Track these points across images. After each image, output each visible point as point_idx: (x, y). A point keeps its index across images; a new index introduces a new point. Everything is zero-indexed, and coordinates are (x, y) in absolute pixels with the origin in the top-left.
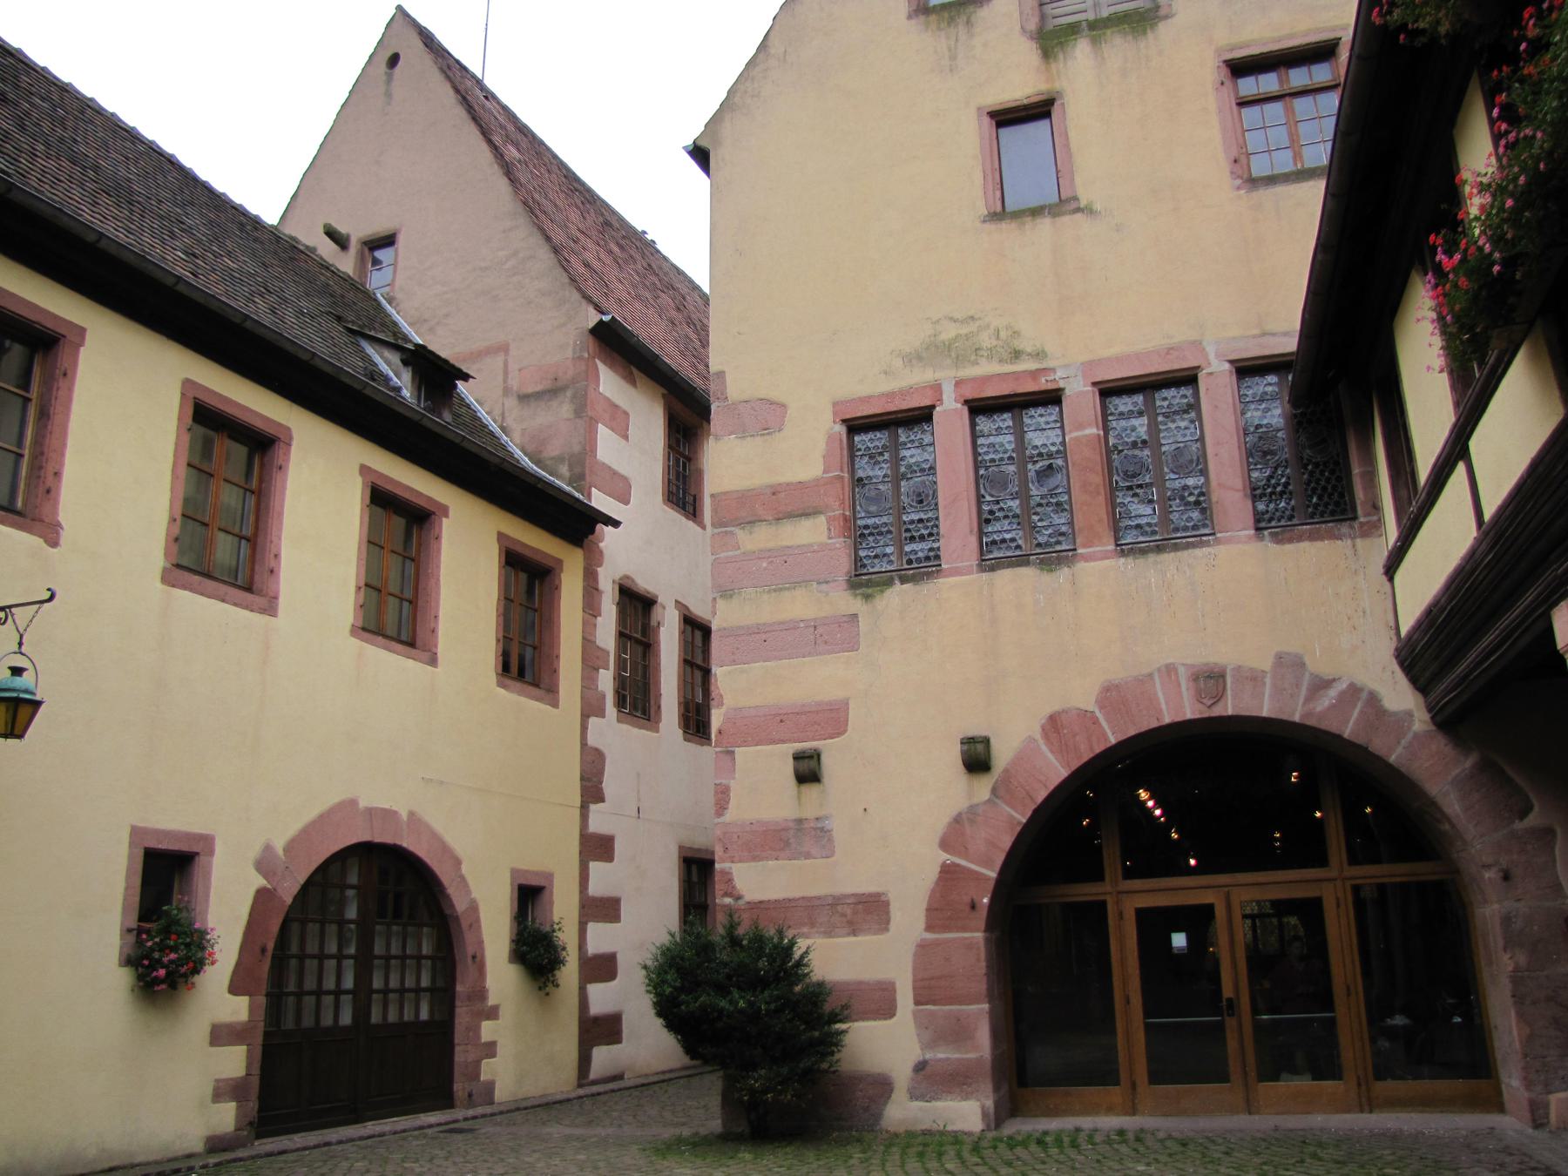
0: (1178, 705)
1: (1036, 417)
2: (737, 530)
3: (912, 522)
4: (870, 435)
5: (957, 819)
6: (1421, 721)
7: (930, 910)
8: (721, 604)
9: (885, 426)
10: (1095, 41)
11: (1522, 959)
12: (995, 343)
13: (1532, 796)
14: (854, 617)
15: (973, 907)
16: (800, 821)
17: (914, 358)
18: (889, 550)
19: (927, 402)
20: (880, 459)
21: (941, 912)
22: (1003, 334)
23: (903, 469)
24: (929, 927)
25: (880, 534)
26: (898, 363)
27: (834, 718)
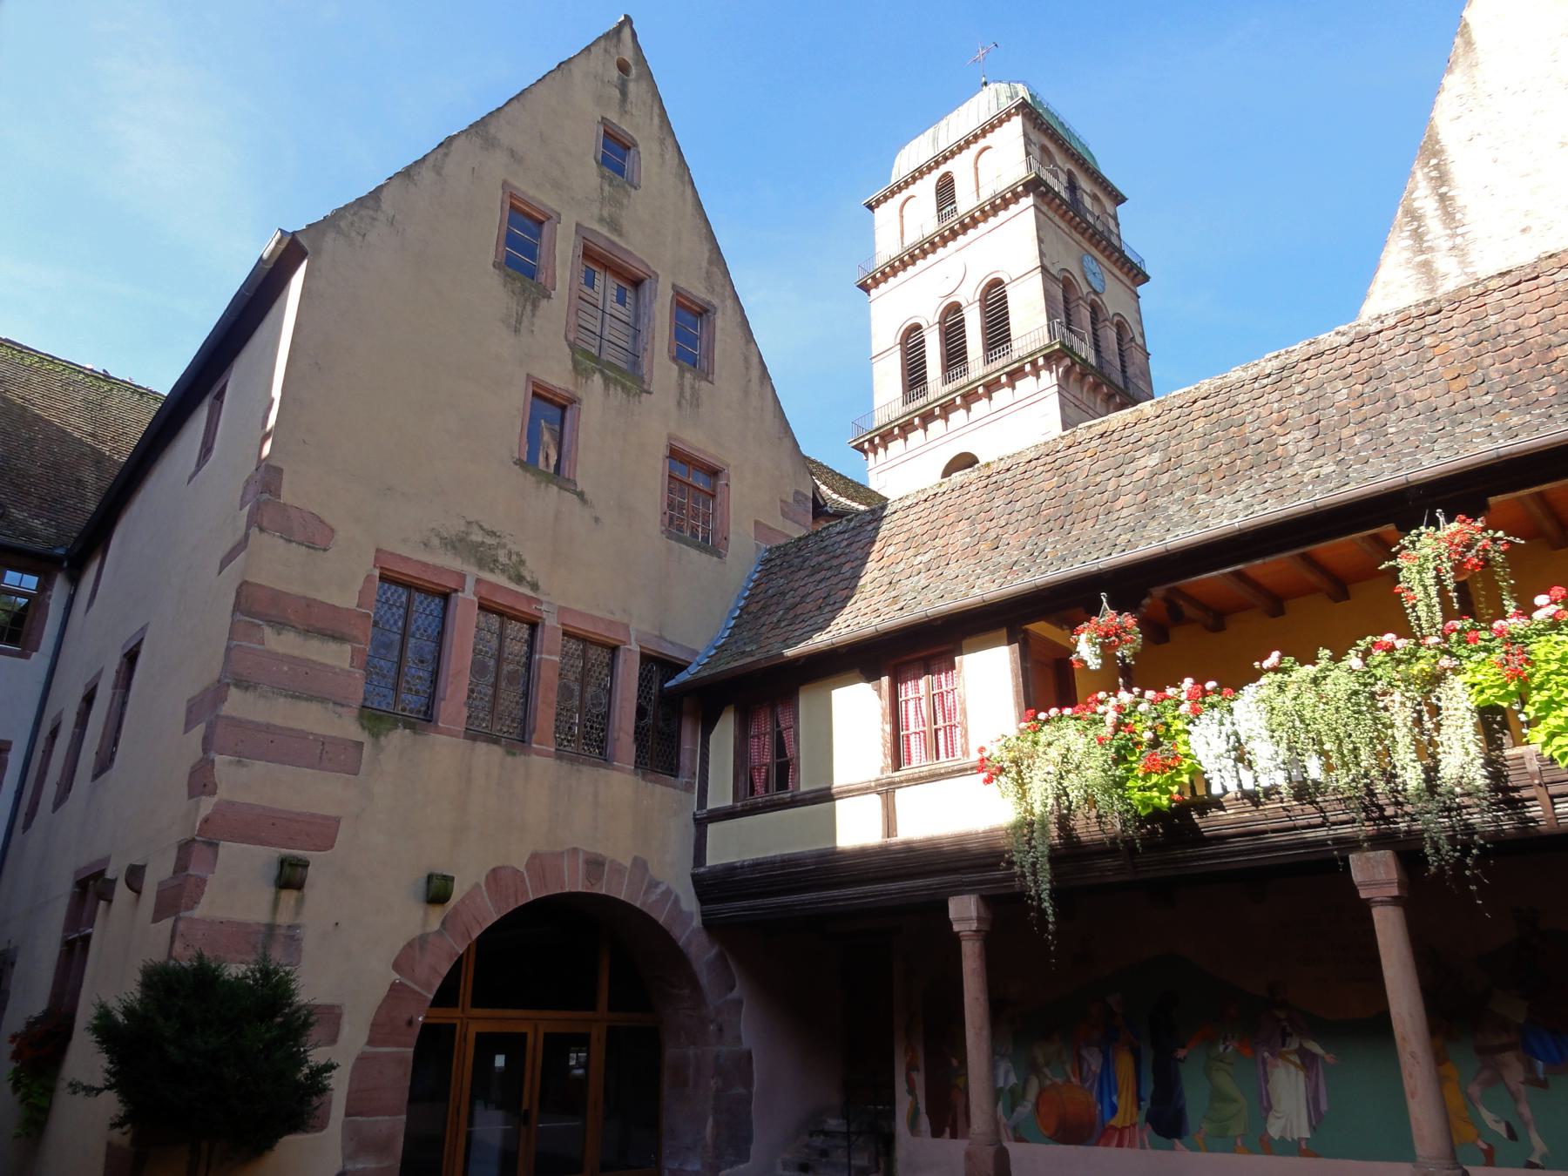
0: (573, 881)
6: (697, 922)
7: (375, 1025)
8: (234, 692)
10: (607, 380)
22: (514, 558)
26: (436, 542)
27: (324, 832)
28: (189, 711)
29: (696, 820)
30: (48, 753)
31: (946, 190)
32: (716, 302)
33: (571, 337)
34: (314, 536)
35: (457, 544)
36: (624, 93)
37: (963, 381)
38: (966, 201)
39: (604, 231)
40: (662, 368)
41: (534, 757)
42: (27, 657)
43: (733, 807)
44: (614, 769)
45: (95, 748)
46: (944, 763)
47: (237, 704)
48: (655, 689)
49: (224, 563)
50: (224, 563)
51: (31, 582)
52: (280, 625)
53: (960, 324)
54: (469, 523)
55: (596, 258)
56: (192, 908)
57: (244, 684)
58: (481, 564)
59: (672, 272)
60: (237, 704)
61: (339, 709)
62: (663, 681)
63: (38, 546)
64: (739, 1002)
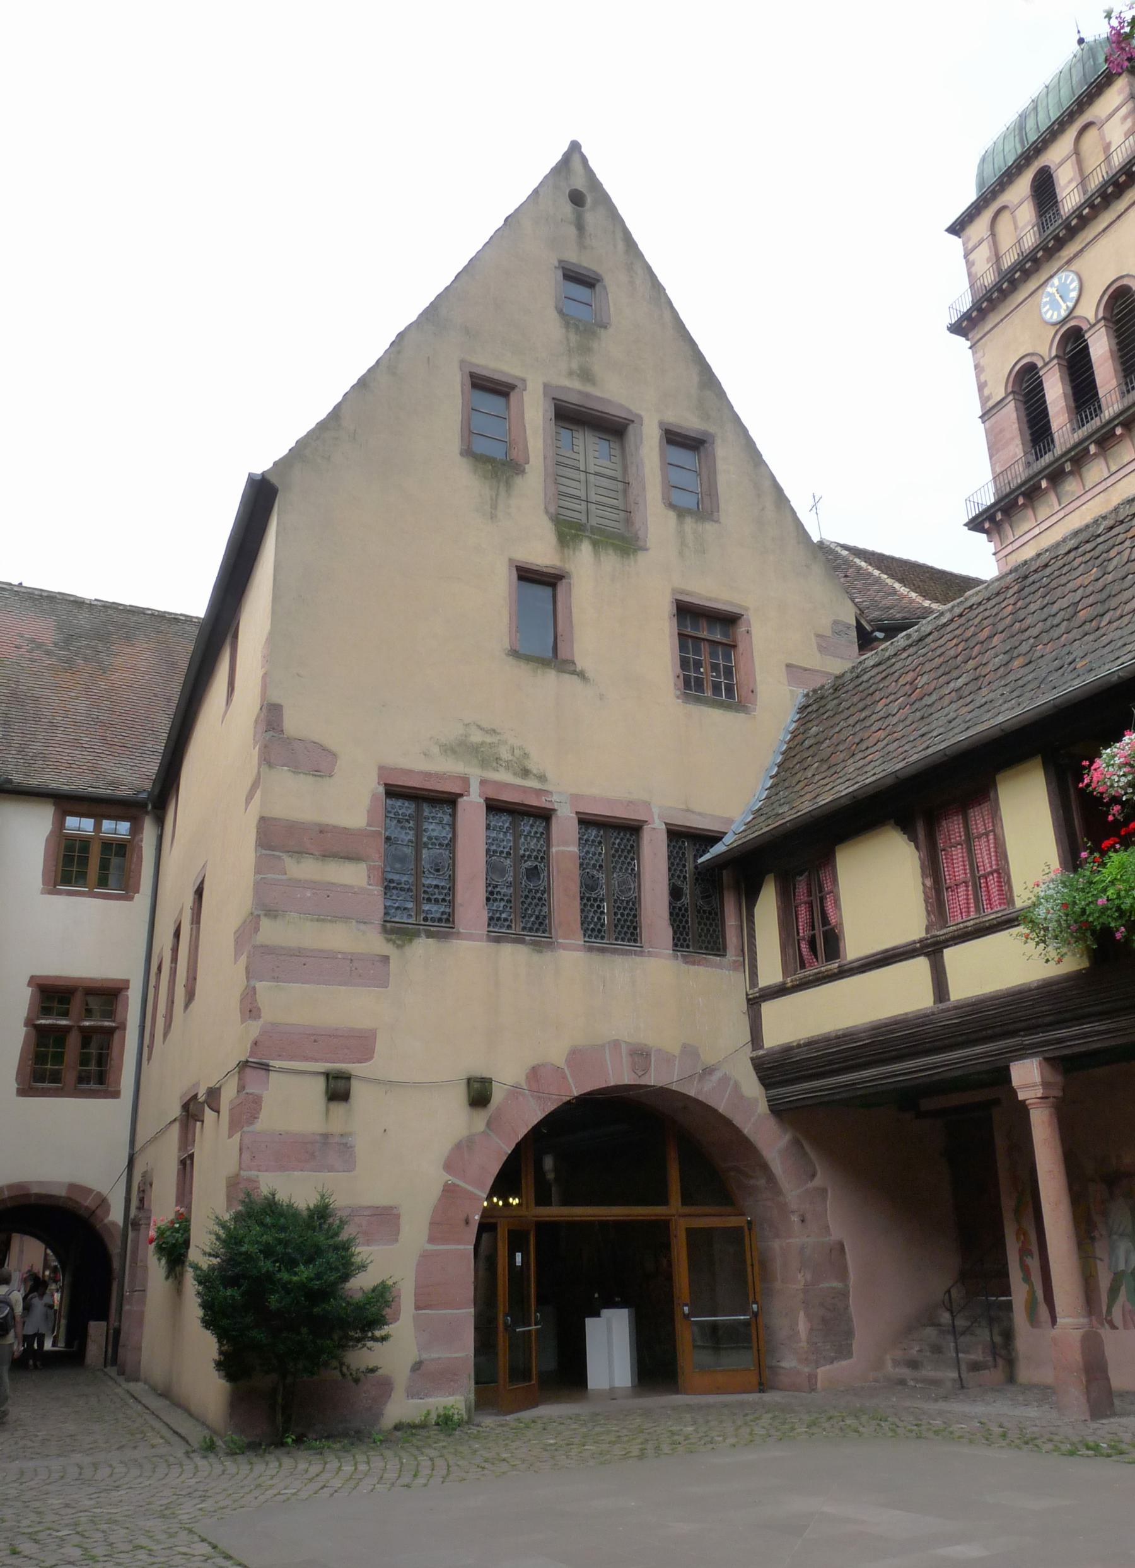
0: (618, 1074)
1: (526, 826)
2: (284, 856)
3: (429, 886)
4: (399, 803)
5: (458, 1147)
6: (763, 1107)
7: (433, 1224)
8: (265, 923)
9: (416, 801)
10: (595, 544)
11: (809, 1277)
12: (511, 758)
13: (818, 1167)
14: (386, 959)
15: (467, 1222)
16: (326, 1136)
17: (450, 750)
18: (410, 905)
19: (457, 790)
20: (407, 825)
21: (439, 1228)
22: (517, 752)
23: (425, 839)
24: (432, 1240)
25: (402, 889)
26: (436, 750)
27: (362, 1044)
28: (236, 942)
29: (748, 1000)
30: (157, 987)
31: (1044, 191)
32: (712, 429)
33: (552, 510)
34: (316, 761)
35: (460, 748)
36: (580, 227)
37: (1096, 423)
38: (1070, 198)
39: (576, 385)
40: (657, 521)
41: (562, 951)
42: (131, 898)
43: (784, 983)
44: (650, 954)
45: (184, 982)
46: (990, 916)
47: (271, 932)
48: (689, 866)
49: (249, 798)
50: (249, 798)
51: (124, 827)
52: (299, 853)
53: (1085, 351)
54: (467, 725)
55: (571, 416)
56: (252, 1124)
57: (272, 913)
58: (484, 763)
59: (651, 411)
60: (271, 932)
61: (362, 927)
62: (696, 857)
63: (124, 792)
64: (823, 1191)
